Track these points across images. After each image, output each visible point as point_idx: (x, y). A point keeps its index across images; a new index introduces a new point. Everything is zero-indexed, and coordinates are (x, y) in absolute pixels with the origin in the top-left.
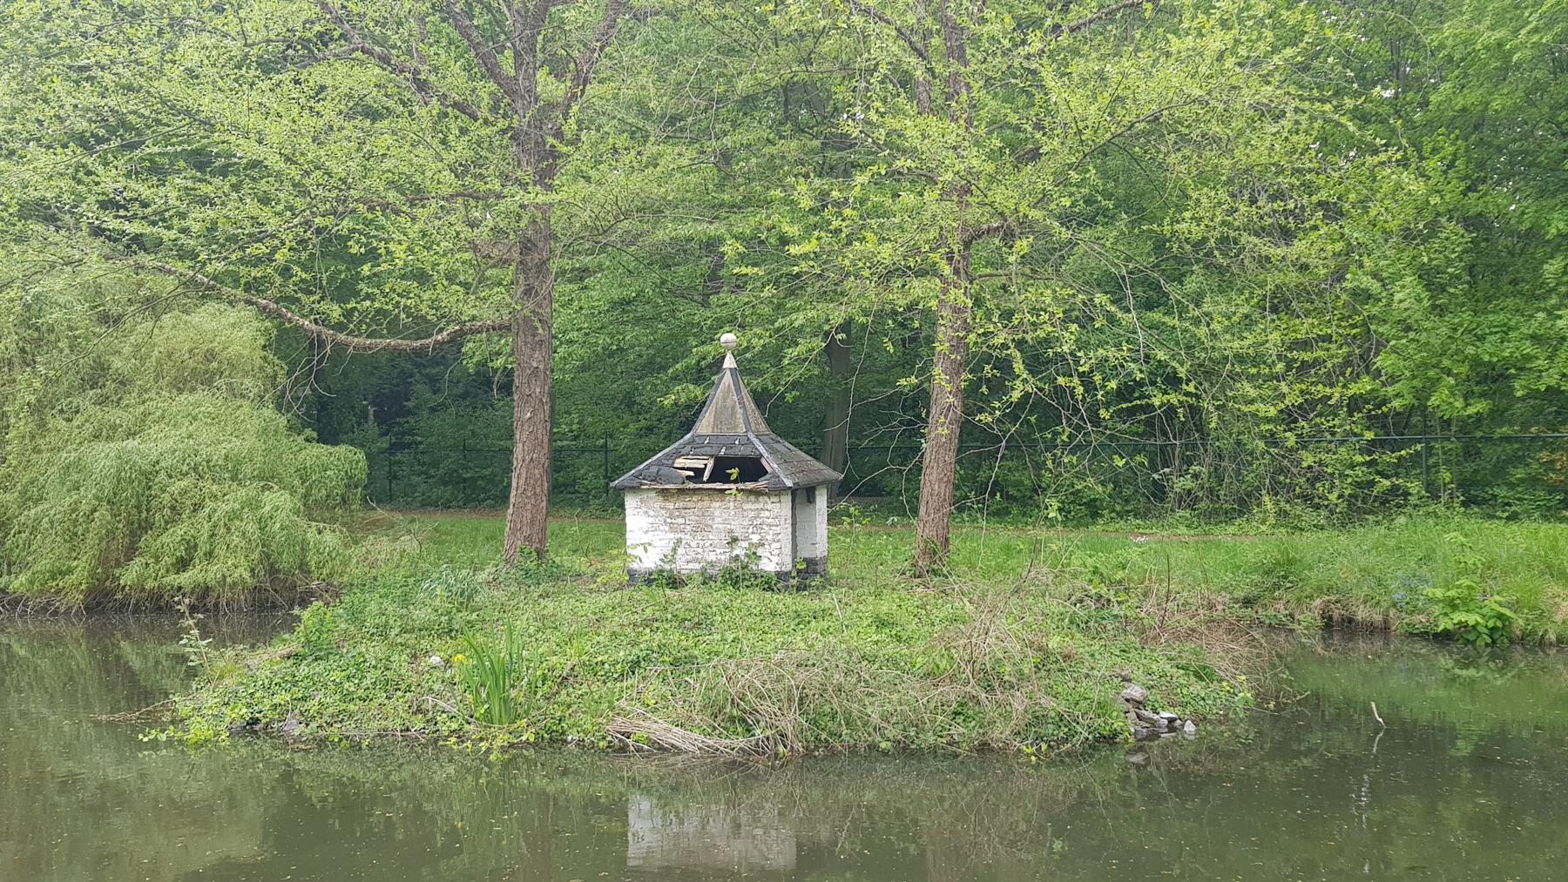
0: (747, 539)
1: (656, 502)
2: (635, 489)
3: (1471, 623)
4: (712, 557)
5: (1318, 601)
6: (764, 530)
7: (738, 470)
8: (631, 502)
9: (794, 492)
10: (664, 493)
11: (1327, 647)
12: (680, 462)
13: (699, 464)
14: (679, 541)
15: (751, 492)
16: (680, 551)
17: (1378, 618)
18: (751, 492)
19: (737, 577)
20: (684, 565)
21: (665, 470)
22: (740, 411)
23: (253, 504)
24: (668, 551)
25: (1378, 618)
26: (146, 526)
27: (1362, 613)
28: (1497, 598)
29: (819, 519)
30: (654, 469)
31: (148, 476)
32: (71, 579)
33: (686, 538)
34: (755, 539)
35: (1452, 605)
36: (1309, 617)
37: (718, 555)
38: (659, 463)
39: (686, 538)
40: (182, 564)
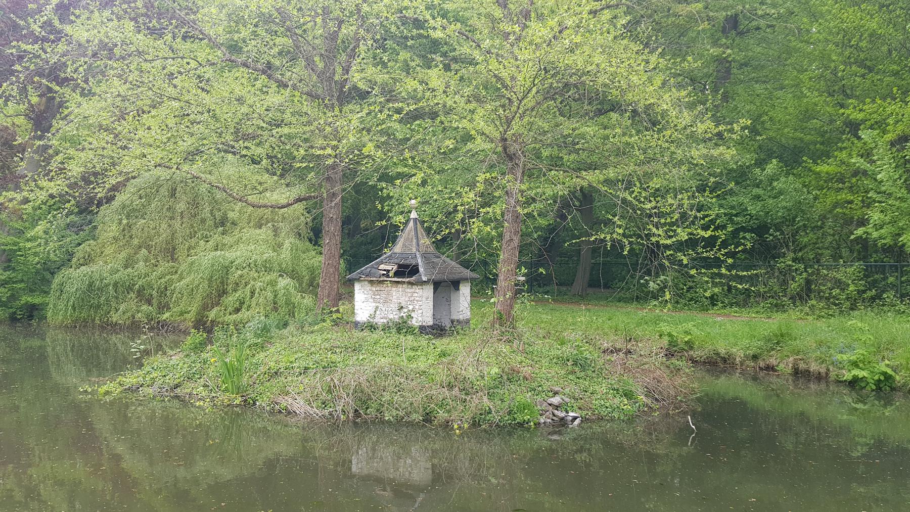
0: (407, 307)
1: (368, 286)
2: (358, 280)
3: (860, 376)
4: (391, 316)
5: (791, 359)
6: (420, 304)
7: (406, 271)
8: (357, 286)
9: (437, 285)
10: (371, 282)
11: (796, 386)
12: (382, 267)
13: (389, 268)
14: (377, 308)
15: (409, 283)
16: (378, 312)
17: (823, 371)
18: (409, 283)
19: (402, 327)
20: (379, 320)
21: (373, 270)
22: (415, 241)
23: (273, 283)
24: (372, 313)
25: (823, 371)
26: (225, 292)
27: (814, 367)
28: (887, 362)
29: (462, 299)
30: (368, 270)
31: (227, 269)
32: (188, 316)
33: (380, 306)
34: (411, 307)
35: (855, 364)
36: (785, 367)
37: (394, 316)
38: (372, 267)
39: (380, 306)
40: (237, 310)
